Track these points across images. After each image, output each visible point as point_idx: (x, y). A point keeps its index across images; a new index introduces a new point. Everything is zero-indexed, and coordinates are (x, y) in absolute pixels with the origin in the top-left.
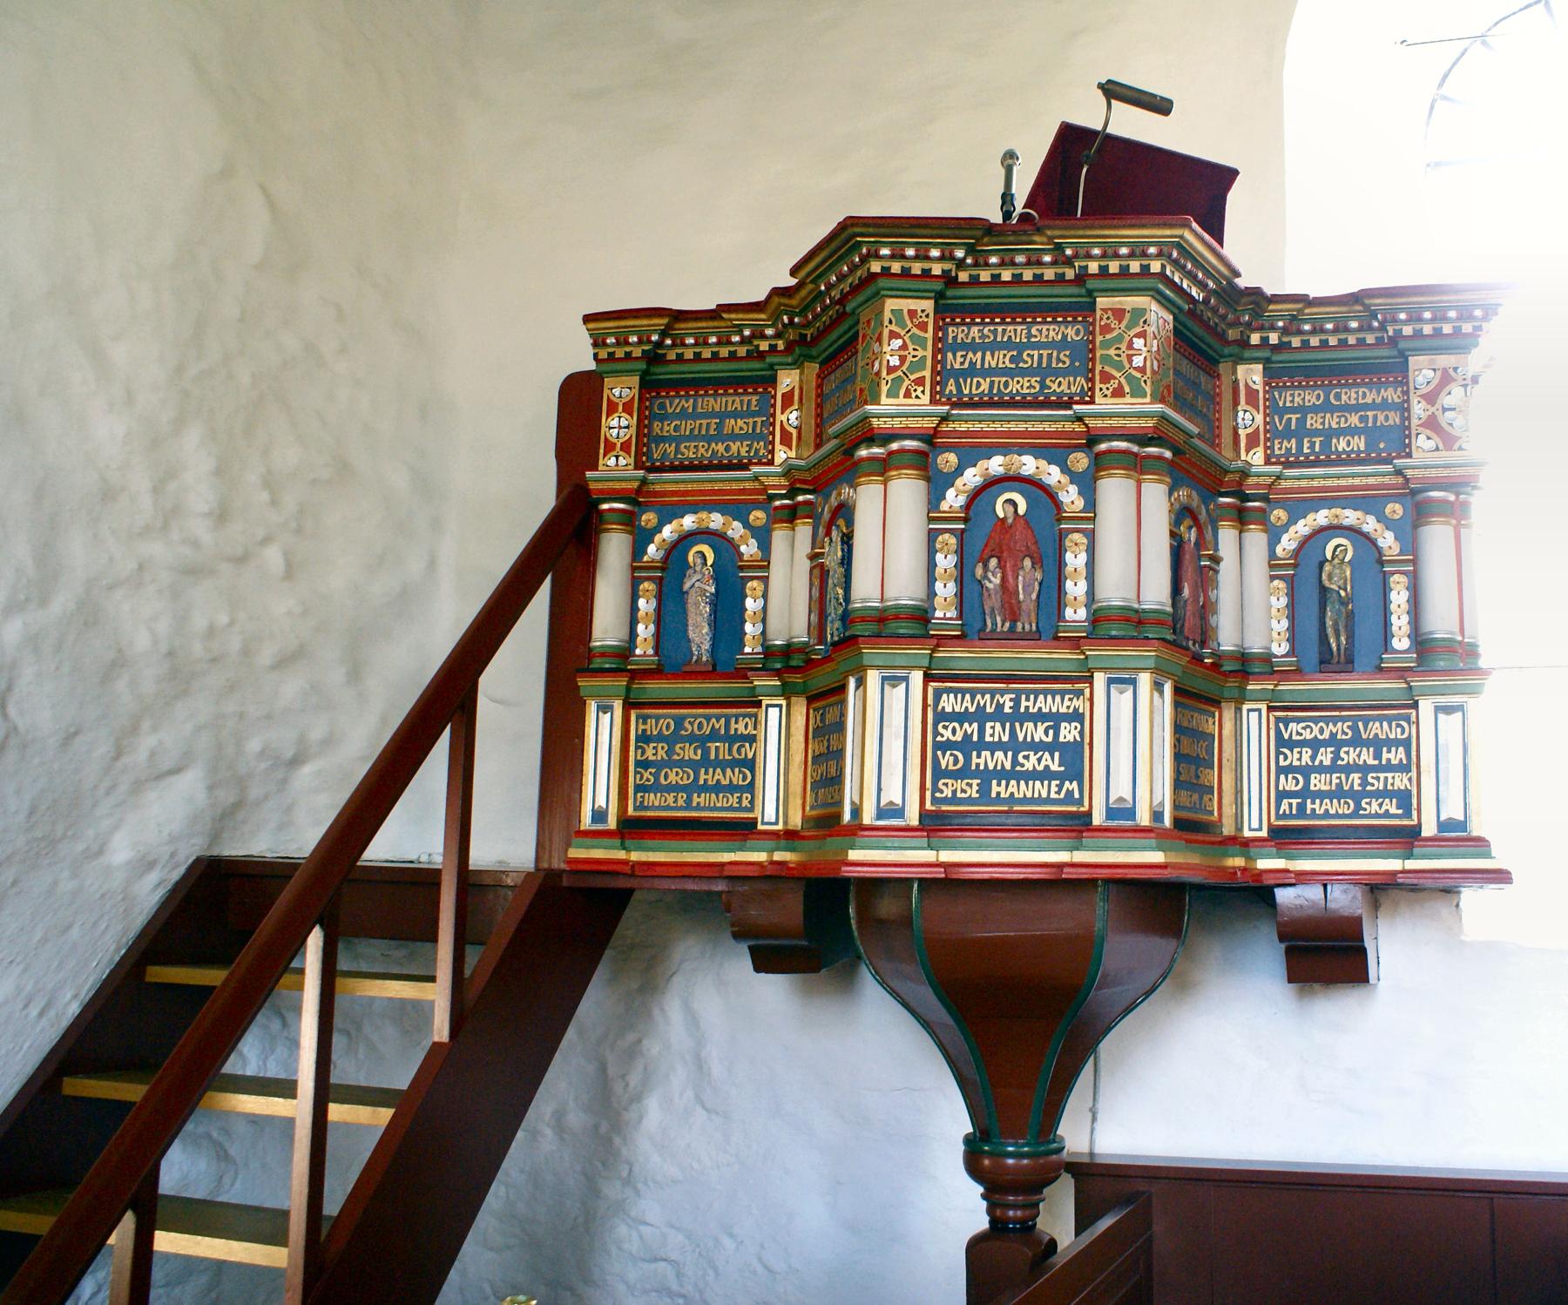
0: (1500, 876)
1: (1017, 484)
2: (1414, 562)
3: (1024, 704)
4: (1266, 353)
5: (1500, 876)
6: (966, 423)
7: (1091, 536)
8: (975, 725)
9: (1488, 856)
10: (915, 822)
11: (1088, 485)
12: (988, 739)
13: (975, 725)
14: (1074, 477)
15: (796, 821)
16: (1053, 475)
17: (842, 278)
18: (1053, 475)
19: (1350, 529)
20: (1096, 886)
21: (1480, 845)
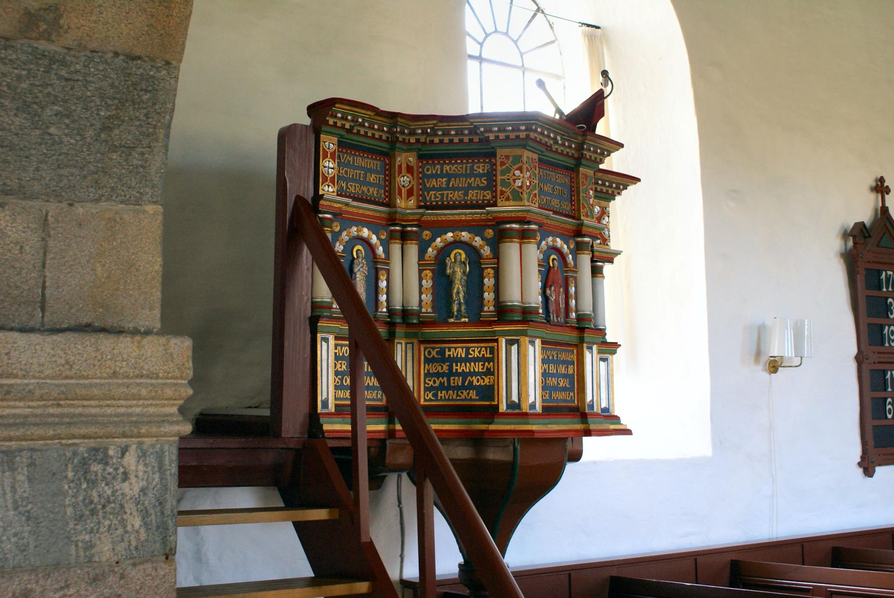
0: (628, 432)
1: (365, 244)
2: (498, 263)
3: (454, 367)
4: (343, 133)
5: (628, 432)
6: (431, 215)
7: (388, 271)
8: (445, 378)
9: (619, 423)
10: (333, 410)
11: (496, 244)
12: (452, 385)
13: (445, 378)
14: (488, 242)
15: (349, 420)
16: (478, 241)
17: (542, 133)
18: (478, 241)
19: (465, 243)
20: (569, 455)
21: (617, 418)
